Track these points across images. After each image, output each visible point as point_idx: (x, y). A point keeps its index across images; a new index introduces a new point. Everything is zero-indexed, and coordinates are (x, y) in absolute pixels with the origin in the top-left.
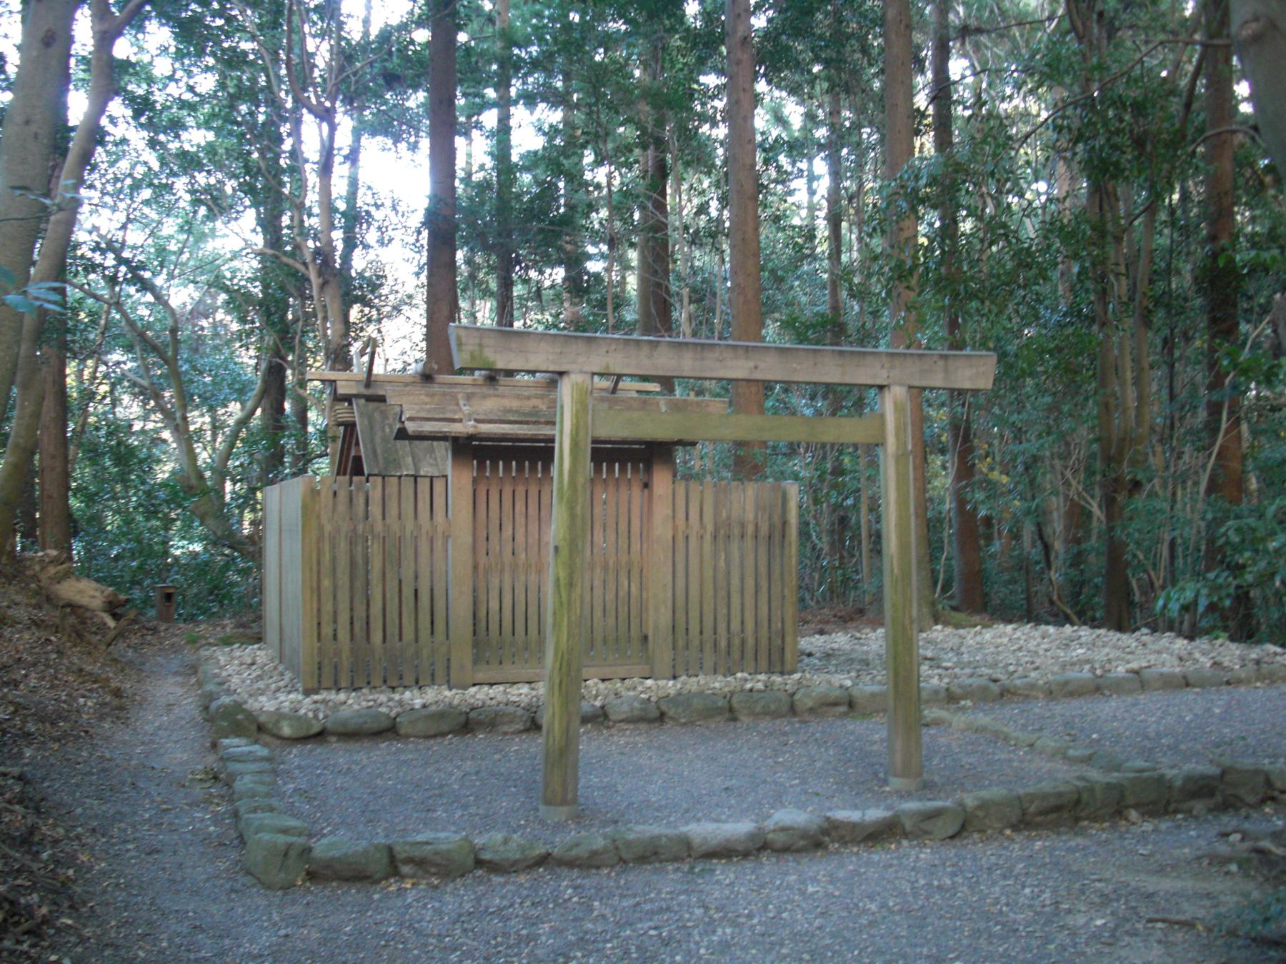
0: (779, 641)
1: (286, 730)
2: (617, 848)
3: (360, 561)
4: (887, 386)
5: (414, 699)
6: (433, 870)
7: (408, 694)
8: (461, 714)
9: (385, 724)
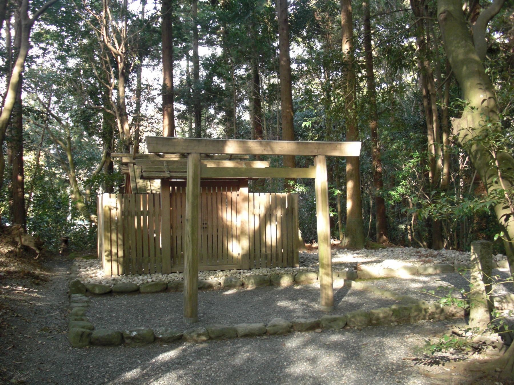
0: (292, 255)
1: (97, 291)
2: (208, 333)
3: (126, 226)
4: (317, 155)
5: (149, 279)
6: (138, 341)
7: (146, 277)
8: (164, 284)
9: (135, 288)
